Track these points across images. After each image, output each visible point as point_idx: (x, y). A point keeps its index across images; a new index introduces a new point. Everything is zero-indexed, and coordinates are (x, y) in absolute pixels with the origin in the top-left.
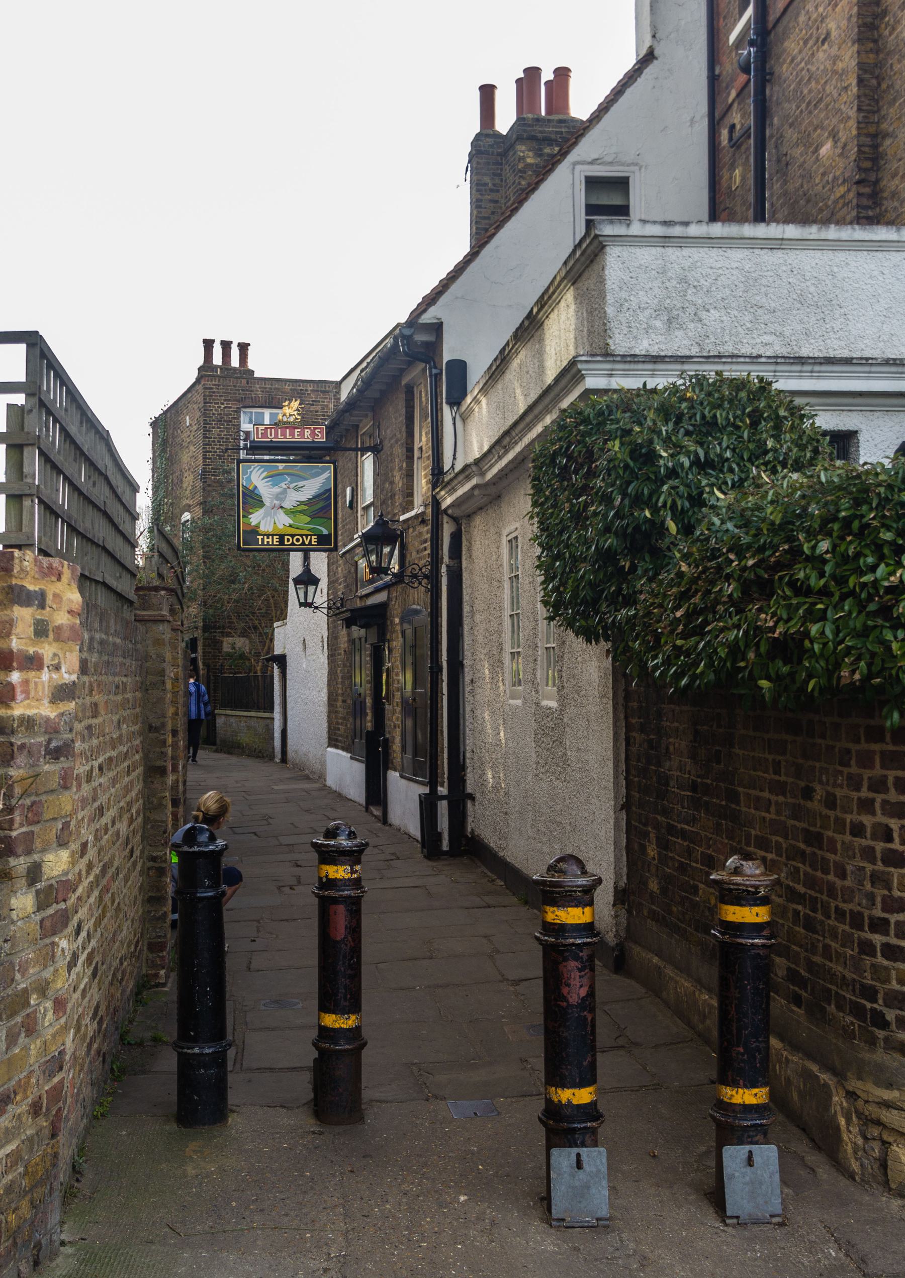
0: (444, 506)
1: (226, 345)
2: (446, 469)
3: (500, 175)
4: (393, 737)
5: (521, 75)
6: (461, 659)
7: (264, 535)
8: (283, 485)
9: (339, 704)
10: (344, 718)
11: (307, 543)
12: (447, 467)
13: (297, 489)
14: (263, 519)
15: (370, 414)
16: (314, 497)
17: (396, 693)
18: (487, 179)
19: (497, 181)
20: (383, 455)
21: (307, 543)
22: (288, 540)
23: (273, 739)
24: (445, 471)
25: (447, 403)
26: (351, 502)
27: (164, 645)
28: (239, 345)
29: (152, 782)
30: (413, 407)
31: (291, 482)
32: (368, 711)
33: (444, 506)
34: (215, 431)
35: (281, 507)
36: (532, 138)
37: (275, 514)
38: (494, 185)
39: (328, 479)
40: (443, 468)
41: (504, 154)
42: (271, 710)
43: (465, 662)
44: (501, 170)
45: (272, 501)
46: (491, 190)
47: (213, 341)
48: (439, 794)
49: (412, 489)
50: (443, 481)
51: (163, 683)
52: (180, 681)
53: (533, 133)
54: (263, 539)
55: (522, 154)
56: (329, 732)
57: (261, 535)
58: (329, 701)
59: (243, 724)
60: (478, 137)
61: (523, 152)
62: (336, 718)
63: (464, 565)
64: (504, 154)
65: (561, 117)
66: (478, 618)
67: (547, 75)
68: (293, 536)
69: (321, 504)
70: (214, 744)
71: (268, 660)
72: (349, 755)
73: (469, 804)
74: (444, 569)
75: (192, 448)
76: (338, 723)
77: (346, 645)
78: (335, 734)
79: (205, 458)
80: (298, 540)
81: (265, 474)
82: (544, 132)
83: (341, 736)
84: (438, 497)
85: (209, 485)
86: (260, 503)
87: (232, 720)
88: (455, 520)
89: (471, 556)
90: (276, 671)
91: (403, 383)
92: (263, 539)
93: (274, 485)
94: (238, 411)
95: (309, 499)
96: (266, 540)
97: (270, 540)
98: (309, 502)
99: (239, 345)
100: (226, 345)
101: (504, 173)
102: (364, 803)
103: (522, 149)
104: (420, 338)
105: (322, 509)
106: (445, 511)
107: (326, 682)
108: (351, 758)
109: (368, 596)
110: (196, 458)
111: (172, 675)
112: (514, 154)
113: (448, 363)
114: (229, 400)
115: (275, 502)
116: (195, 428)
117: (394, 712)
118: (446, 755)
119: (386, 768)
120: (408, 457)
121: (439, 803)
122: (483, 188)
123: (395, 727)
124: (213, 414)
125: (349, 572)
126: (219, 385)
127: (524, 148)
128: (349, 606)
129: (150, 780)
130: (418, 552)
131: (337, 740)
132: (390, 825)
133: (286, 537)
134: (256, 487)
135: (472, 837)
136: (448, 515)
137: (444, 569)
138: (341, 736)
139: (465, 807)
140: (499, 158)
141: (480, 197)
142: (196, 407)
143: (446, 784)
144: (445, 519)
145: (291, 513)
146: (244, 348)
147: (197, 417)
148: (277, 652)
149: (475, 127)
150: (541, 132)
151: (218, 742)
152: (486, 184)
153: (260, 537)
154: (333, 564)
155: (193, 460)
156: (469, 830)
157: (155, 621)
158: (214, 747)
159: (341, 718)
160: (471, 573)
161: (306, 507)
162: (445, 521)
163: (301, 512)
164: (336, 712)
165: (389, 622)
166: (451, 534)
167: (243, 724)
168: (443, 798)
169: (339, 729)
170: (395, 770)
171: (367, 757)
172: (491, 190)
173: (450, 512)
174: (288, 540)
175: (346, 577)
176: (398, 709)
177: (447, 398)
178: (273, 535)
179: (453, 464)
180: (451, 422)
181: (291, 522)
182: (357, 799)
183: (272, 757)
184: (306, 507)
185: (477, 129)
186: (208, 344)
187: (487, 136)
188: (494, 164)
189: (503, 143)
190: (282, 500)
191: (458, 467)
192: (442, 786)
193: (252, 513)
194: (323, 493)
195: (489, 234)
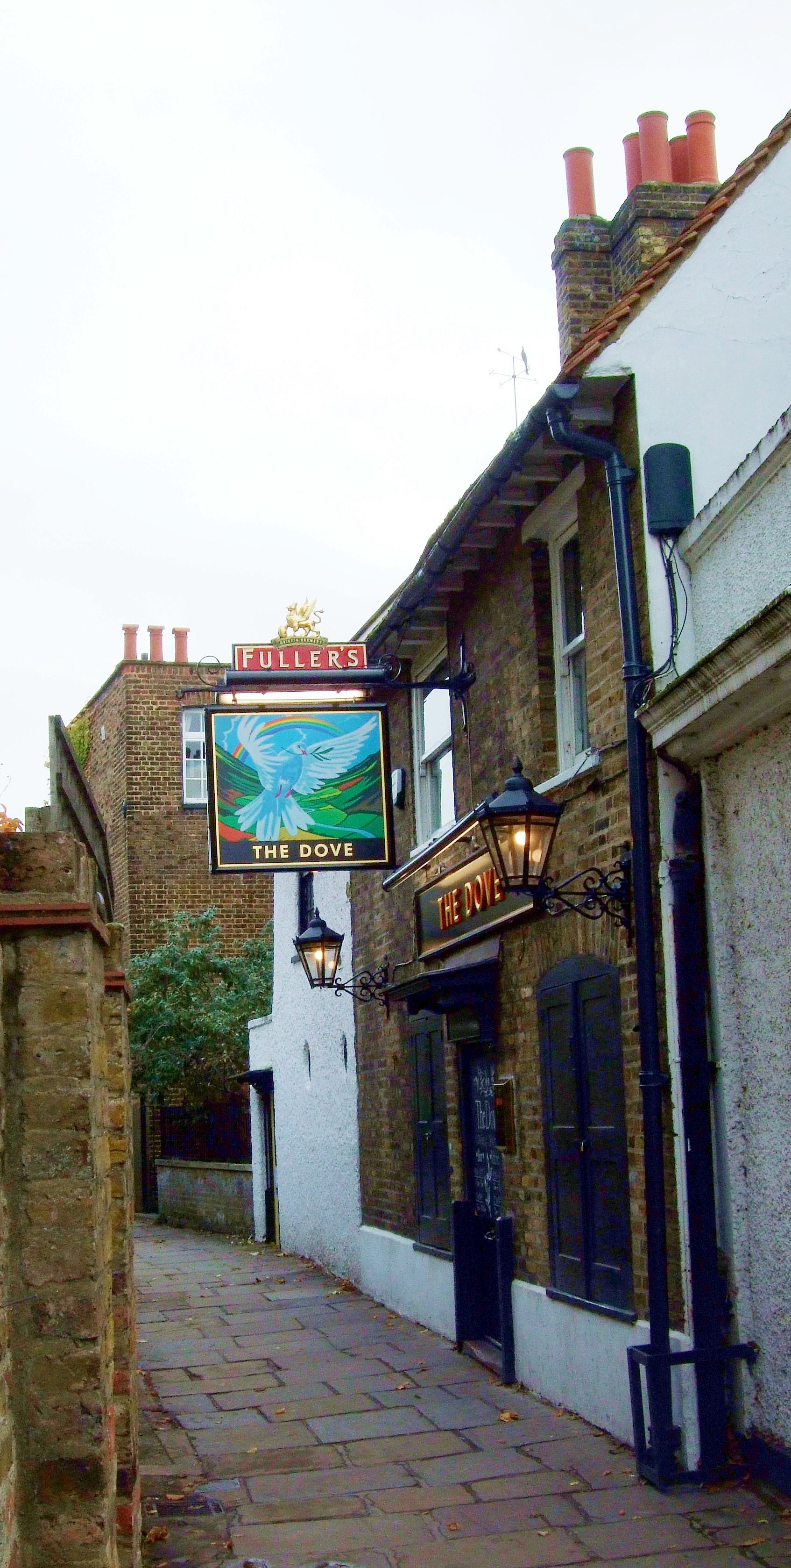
0: (658, 739)
1: (156, 634)
2: (657, 664)
3: (606, 282)
4: (526, 1217)
5: (635, 128)
6: (710, 1058)
7: (263, 844)
8: (294, 747)
9: (385, 1150)
10: (397, 1177)
11: (336, 854)
12: (659, 660)
13: (320, 755)
14: (261, 817)
15: (440, 630)
16: (351, 771)
17: (529, 1133)
18: (586, 289)
19: (603, 290)
20: (475, 691)
21: (336, 854)
22: (306, 851)
23: (250, 1203)
24: (656, 669)
25: (653, 532)
26: (402, 795)
27: (84, 1013)
28: (175, 632)
29: (51, 1518)
30: (548, 581)
31: (309, 742)
32: (453, 1164)
33: (658, 739)
34: (145, 745)
35: (293, 793)
36: (660, 217)
37: (282, 806)
38: (598, 297)
39: (374, 732)
40: (649, 662)
41: (612, 251)
42: (245, 1155)
43: (721, 1064)
44: (609, 274)
45: (276, 781)
46: (595, 305)
47: (136, 628)
48: (674, 1349)
49: (554, 736)
50: (652, 693)
51: (84, 1151)
52: (127, 1132)
53: (662, 208)
54: (262, 852)
55: (646, 241)
56: (363, 1199)
57: (258, 843)
58: (361, 1147)
59: (200, 1181)
60: (567, 226)
61: (648, 237)
62: (379, 1175)
63: (710, 856)
64: (612, 251)
65: (702, 184)
66: (753, 967)
67: (676, 129)
68: (313, 843)
69: (363, 786)
70: (155, 1210)
71: (241, 1080)
72: (410, 1242)
73: (743, 1367)
74: (663, 871)
75: (110, 771)
76: (382, 1185)
77: (397, 1047)
78: (376, 1203)
79: (130, 784)
80: (321, 850)
81: (261, 728)
82: (681, 207)
83: (389, 1206)
84: (645, 723)
85: (138, 824)
86: (255, 786)
87: (184, 1175)
88: (680, 766)
89: (723, 842)
90: (253, 1091)
91: (524, 538)
92: (262, 852)
93: (281, 747)
94: (177, 714)
95: (342, 776)
96: (267, 852)
97: (274, 852)
98: (342, 781)
99: (175, 632)
100: (156, 634)
101: (612, 279)
102: (452, 1334)
103: (645, 233)
104: (583, 416)
105: (366, 794)
106: (662, 749)
107: (355, 1115)
108: (416, 1248)
109: (444, 955)
110: (117, 785)
111: (107, 1120)
112: (634, 241)
113: (654, 452)
114: (165, 698)
115: (282, 782)
116: (115, 741)
117: (525, 1169)
118: (685, 1262)
119: (510, 1276)
120: (542, 675)
121: (674, 1369)
122: (581, 302)
123: (528, 1198)
124: (141, 718)
125: (401, 918)
126: (148, 677)
127: (648, 231)
128: (400, 978)
129: (40, 1510)
130: (581, 850)
131: (381, 1214)
132: (523, 1389)
133: (302, 847)
134: (246, 754)
135: (755, 1438)
136: (668, 760)
137: (663, 871)
138: (389, 1206)
139: (733, 1374)
140: (603, 257)
141: (576, 315)
142: (114, 710)
143: (688, 1325)
144: (661, 768)
145: (309, 803)
146: (180, 636)
147: (117, 724)
148: (256, 1064)
149: (562, 212)
150: (673, 207)
151: (160, 1207)
152: (583, 297)
153: (257, 848)
154: (362, 910)
155: (113, 788)
156: (747, 1424)
157: (55, 931)
158: (154, 1216)
159: (390, 1176)
160: (727, 876)
161: (338, 792)
162: (660, 771)
163: (327, 802)
164: (379, 1165)
165: (504, 998)
166: (679, 797)
167: (200, 1181)
168: (683, 1357)
169: (385, 1195)
170: (532, 1280)
171: (458, 1251)
172: (595, 305)
173: (674, 751)
174: (306, 851)
175: (392, 931)
176: (537, 1164)
177: (650, 523)
178: (279, 843)
179: (672, 655)
180: (662, 572)
181: (312, 822)
182: (442, 1330)
183: (248, 1230)
184: (338, 792)
185: (564, 214)
186: (130, 632)
187: (583, 223)
188: (596, 265)
189: (609, 232)
190: (294, 778)
191: (684, 665)
192: (679, 1326)
193: (241, 807)
194: (366, 763)
195: (716, 204)
